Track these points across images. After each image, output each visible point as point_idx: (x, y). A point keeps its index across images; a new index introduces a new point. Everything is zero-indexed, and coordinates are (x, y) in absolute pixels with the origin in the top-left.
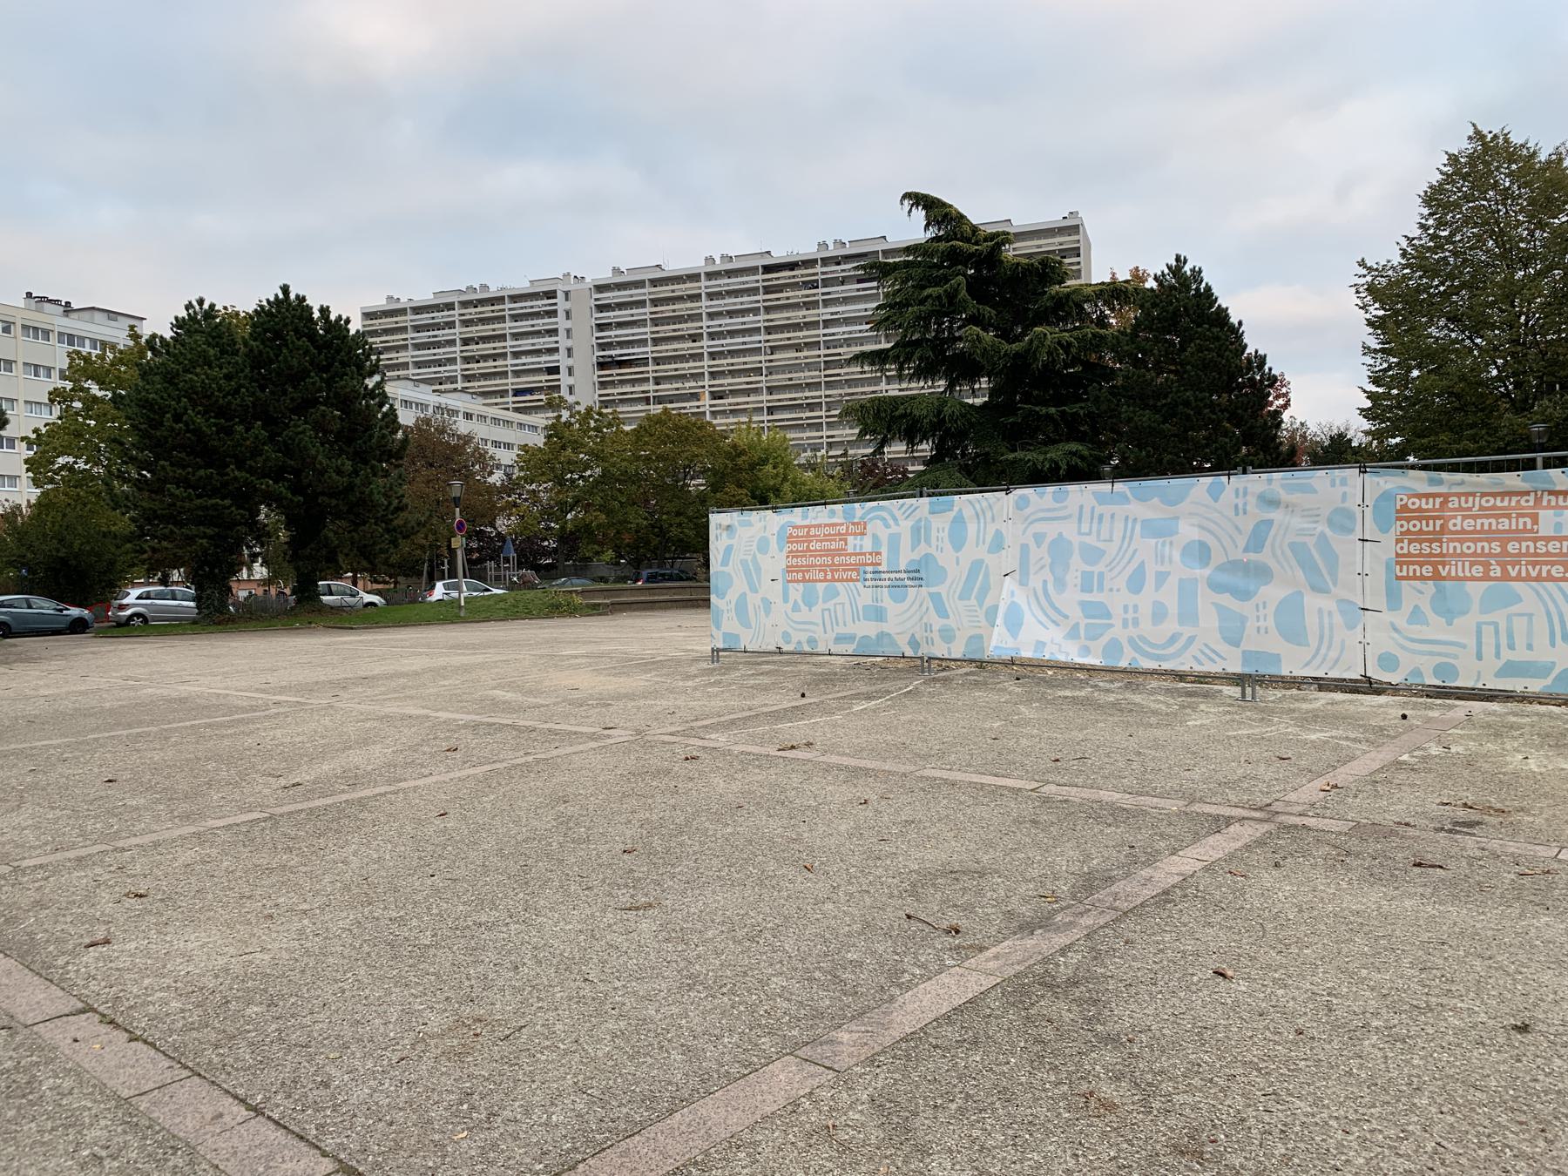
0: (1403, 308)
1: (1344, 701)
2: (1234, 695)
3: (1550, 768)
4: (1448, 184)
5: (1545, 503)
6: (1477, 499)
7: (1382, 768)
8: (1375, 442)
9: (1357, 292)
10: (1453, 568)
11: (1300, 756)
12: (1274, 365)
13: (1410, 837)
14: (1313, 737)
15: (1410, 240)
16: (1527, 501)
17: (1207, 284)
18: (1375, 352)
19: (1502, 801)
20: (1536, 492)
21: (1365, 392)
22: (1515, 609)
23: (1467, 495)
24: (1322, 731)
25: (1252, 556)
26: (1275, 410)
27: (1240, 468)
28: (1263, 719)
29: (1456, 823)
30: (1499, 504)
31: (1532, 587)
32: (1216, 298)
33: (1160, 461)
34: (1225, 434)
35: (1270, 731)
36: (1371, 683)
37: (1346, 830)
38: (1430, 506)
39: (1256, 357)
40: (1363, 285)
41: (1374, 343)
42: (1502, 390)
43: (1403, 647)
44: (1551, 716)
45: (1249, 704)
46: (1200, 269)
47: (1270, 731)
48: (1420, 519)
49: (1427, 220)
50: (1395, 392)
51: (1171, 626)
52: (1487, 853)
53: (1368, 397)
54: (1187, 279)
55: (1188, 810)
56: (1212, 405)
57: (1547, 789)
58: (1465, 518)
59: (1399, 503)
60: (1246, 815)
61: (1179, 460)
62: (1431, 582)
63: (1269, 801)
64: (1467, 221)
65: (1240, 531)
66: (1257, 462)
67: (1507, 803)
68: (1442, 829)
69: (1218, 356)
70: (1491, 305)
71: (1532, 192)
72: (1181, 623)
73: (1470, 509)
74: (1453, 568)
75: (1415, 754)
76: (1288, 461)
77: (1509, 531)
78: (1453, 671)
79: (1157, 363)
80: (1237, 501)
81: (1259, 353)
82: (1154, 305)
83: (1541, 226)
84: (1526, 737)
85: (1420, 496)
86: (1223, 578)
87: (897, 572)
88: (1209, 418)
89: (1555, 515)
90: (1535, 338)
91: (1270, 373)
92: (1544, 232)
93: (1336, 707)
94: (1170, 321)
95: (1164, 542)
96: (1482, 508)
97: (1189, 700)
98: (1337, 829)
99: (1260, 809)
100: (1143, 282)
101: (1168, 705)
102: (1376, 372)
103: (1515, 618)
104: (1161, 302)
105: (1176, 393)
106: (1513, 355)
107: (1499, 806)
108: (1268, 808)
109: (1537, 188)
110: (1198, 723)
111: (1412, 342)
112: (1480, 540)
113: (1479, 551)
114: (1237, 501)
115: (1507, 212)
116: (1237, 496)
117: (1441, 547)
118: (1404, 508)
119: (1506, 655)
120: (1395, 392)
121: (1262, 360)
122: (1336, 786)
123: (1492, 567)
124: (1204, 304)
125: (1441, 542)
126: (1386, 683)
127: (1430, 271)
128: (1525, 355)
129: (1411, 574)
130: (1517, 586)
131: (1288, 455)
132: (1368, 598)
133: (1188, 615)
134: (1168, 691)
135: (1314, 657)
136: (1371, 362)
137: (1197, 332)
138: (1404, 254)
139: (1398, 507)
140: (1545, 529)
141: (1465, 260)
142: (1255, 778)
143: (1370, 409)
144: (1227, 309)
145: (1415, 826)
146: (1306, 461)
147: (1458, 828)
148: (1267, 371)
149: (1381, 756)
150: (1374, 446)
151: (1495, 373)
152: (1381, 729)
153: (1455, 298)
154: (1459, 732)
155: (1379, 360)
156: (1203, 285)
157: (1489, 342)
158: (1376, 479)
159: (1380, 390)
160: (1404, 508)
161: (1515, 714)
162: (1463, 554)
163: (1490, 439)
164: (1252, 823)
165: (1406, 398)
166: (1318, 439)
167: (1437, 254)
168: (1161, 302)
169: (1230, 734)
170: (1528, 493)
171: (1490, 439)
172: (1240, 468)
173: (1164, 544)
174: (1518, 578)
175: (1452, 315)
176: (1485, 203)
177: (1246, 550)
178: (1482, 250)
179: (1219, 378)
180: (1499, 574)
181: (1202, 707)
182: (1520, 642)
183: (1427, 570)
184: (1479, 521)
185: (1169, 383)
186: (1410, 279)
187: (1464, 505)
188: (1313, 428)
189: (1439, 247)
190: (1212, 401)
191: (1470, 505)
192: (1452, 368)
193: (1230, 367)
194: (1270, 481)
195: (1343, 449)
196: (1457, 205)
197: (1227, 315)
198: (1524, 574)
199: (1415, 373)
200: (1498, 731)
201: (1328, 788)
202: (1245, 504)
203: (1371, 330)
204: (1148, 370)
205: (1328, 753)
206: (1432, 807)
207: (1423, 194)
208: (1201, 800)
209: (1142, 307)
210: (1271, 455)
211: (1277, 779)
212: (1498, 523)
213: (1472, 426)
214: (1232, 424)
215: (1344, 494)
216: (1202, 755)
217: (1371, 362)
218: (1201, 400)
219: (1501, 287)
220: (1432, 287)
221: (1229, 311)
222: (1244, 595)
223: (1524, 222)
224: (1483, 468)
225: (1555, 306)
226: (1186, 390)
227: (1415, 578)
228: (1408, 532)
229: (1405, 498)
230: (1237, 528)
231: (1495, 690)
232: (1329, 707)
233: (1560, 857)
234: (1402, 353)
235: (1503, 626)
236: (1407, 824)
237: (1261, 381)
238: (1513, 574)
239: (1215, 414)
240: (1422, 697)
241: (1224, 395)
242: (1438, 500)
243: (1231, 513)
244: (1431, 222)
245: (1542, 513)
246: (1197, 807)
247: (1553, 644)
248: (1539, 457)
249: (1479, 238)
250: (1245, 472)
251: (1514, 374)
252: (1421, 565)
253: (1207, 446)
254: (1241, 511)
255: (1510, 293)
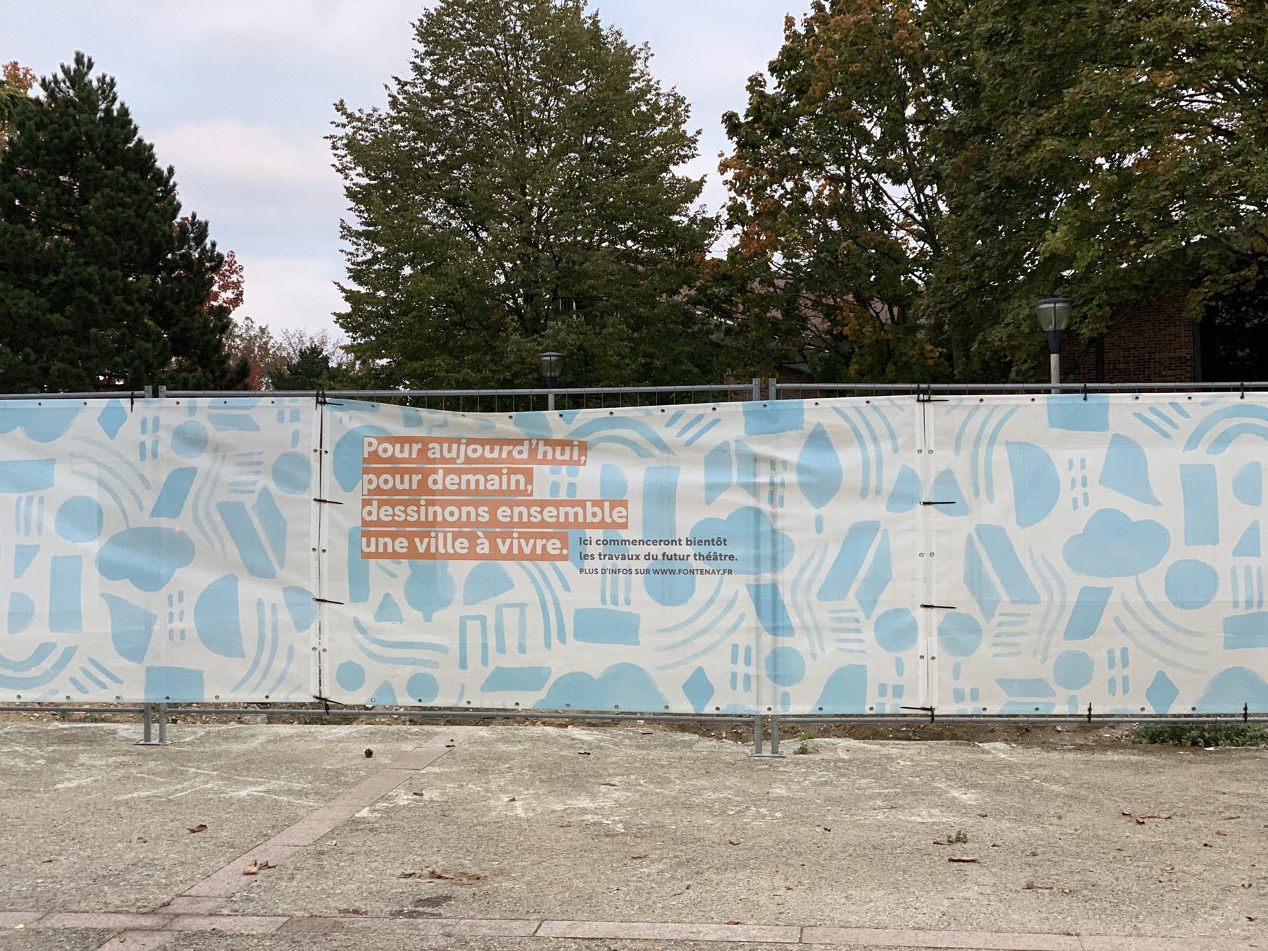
0: (393, 179)
1: (292, 737)
2: (136, 737)
3: (539, 810)
4: (448, 15)
5: (540, 456)
6: (463, 447)
7: (332, 831)
8: (358, 362)
9: (335, 147)
10: (433, 540)
11: (220, 823)
12: (221, 239)
13: (358, 931)
14: (243, 793)
15: (403, 84)
16: (520, 452)
17: (122, 105)
18: (358, 234)
19: (478, 865)
20: (530, 440)
21: (343, 290)
22: (504, 597)
23: (451, 441)
24: (252, 784)
25: (165, 522)
26: (221, 306)
27: (149, 388)
28: (172, 772)
29: (420, 902)
30: (488, 455)
31: (523, 567)
32: (136, 129)
33: (45, 371)
34: (147, 336)
35: (182, 790)
36: (327, 707)
37: (273, 931)
38: (406, 455)
39: (193, 224)
40: (341, 138)
41: (356, 224)
42: (510, 303)
43: (372, 655)
44: (546, 740)
45: (154, 749)
46: (112, 80)
47: (182, 790)
48: (393, 472)
49: (422, 60)
50: (381, 294)
51: (38, 632)
52: (453, 940)
53: (347, 299)
54: (91, 92)
55: (41, 927)
56: (126, 291)
57: (533, 840)
58: (447, 472)
59: (367, 449)
60: (130, 924)
61: (75, 371)
62: (405, 562)
63: (166, 899)
64: (471, 71)
65: (147, 484)
66: (192, 382)
67: (484, 866)
68: (400, 913)
69: (138, 215)
70: (499, 189)
71: (546, 46)
72: (54, 626)
73: (453, 461)
74: (433, 540)
75: (378, 806)
76: (238, 382)
77: (500, 492)
78: (430, 685)
79: (43, 217)
80: (143, 438)
81: (197, 218)
82: (40, 126)
83: (558, 92)
84: (516, 771)
85: (394, 440)
86: (121, 555)
87: (667, 543)
88: (122, 310)
89: (552, 472)
90: (548, 239)
91: (213, 251)
92: (559, 100)
93: (280, 746)
94: (67, 156)
95: (30, 499)
96: (468, 460)
97: (63, 748)
98: (261, 930)
99: (153, 912)
100: (26, 89)
101: (29, 759)
102: (358, 264)
103: (504, 610)
104: (52, 122)
105: (72, 268)
106: (522, 257)
107: (474, 871)
108: (164, 910)
109: (552, 41)
110: (74, 784)
111: (402, 226)
112: (466, 503)
113: (464, 519)
114: (143, 438)
115: (518, 67)
116: (144, 430)
117: (418, 512)
118: (374, 456)
119: (497, 661)
120: (381, 294)
121: (202, 230)
122: (266, 866)
123: (479, 541)
124: (117, 136)
125: (419, 506)
126: (358, 706)
127: (428, 131)
128: (537, 259)
129: (381, 550)
130: (508, 566)
131: (237, 374)
132: (325, 583)
133: (66, 616)
134: (33, 737)
135: (251, 672)
136: (352, 249)
137: (105, 177)
138: (394, 103)
139: (366, 456)
140: (541, 490)
141: (468, 124)
142: (151, 864)
143: (349, 315)
144: (151, 147)
145: (366, 913)
146: (267, 383)
147: (420, 909)
148: (209, 246)
149: (332, 814)
150: (357, 367)
151: (502, 279)
152: (338, 773)
153: (456, 173)
154: (436, 770)
155: (362, 248)
156: (116, 106)
157: (496, 238)
158: (338, 414)
159: (363, 290)
160: (374, 456)
161: (505, 740)
162: (445, 523)
163: (495, 368)
164: (139, 936)
165: (395, 303)
166: (284, 354)
167: (434, 109)
168: (52, 122)
169: (121, 798)
170: (519, 442)
171: (495, 368)
172: (149, 388)
173: (30, 499)
174: (510, 556)
175: (452, 196)
176: (492, 50)
177: (156, 513)
178: (488, 113)
179: (138, 251)
180: (487, 551)
181: (83, 758)
182: (511, 642)
183: (401, 545)
184: (464, 477)
185: (62, 250)
186: (402, 139)
187: (447, 455)
188: (277, 338)
189: (435, 102)
190: (127, 284)
191: (454, 454)
192: (450, 268)
193: (155, 235)
194: (192, 410)
195: (318, 370)
196: (458, 47)
197: (152, 156)
198: (515, 551)
199: (407, 271)
200: (482, 766)
201: (254, 869)
202: (156, 443)
203: (352, 204)
204: (29, 227)
205: (260, 816)
206: (394, 885)
207: (417, 23)
208: (65, 909)
209: (21, 126)
210: (213, 372)
211: (182, 863)
212: (486, 481)
213: (475, 349)
214: (159, 324)
215: (296, 435)
216: (73, 834)
217: (352, 249)
218: (112, 281)
219: (511, 166)
220: (429, 154)
221: (155, 150)
222: (149, 581)
223: (537, 84)
224: (470, 405)
225: (571, 200)
226: (87, 264)
227: (385, 555)
228: (378, 491)
229: (374, 442)
230: (142, 478)
231: (493, 710)
232: (270, 747)
233: (539, 933)
234: (389, 241)
235: (491, 622)
236: (356, 912)
237: (200, 260)
238: (504, 550)
239: (133, 304)
240: (404, 723)
241: (146, 277)
242: (416, 447)
243: (134, 457)
244: (427, 64)
245: (537, 468)
246: (57, 921)
247: (548, 645)
248: (551, 392)
249: (484, 95)
250: (156, 394)
251: (524, 284)
252: (394, 536)
253: (118, 351)
254: (149, 454)
255: (522, 175)
